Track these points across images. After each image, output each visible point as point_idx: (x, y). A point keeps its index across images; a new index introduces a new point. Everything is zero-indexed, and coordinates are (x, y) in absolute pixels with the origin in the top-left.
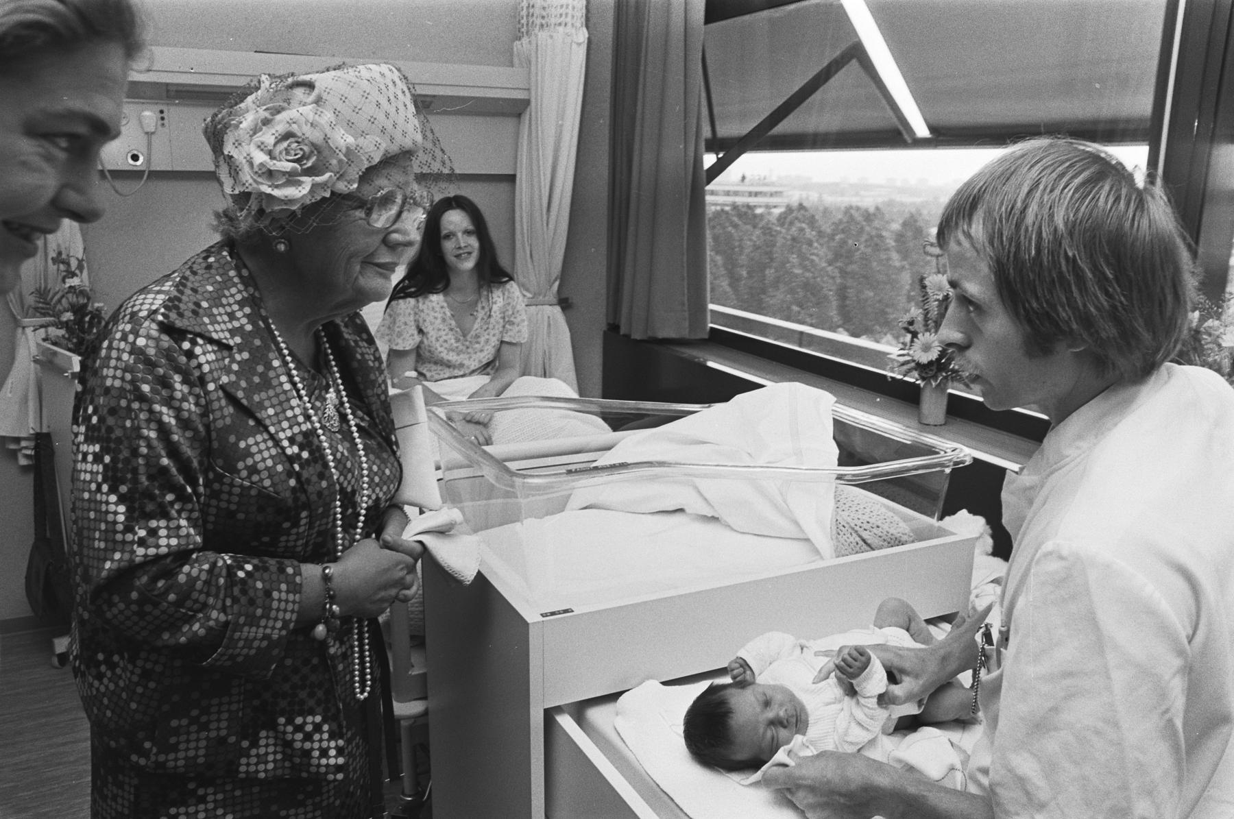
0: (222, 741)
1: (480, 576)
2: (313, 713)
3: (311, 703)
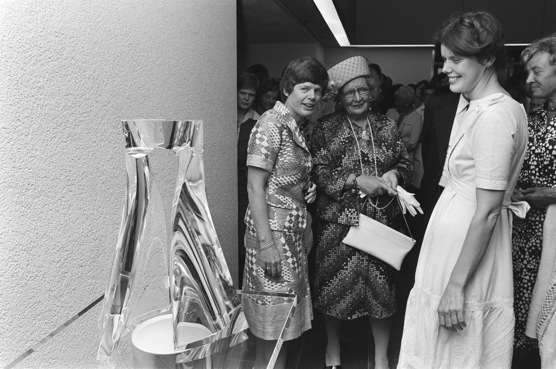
0: (335, 213)
1: (442, 189)
2: (353, 208)
3: (353, 206)
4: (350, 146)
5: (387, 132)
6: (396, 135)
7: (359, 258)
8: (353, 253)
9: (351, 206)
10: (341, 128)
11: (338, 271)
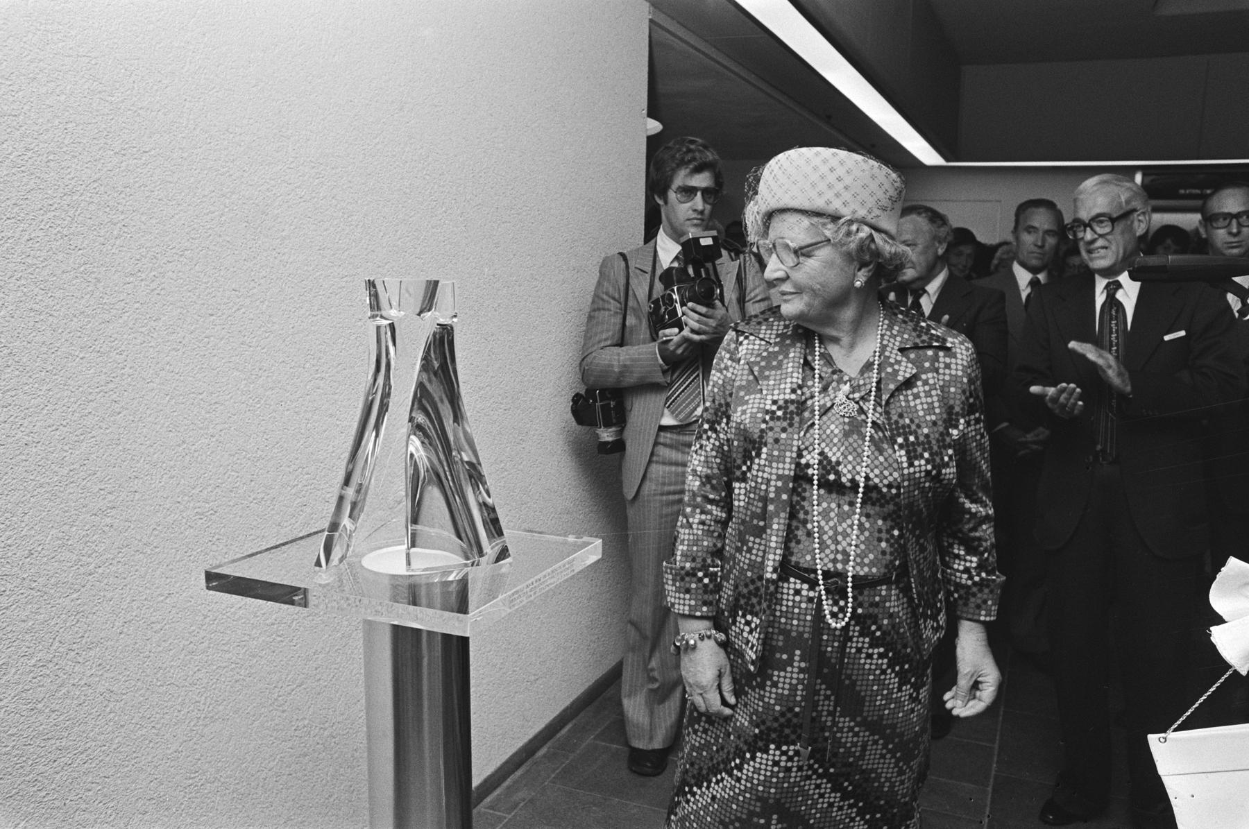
4: (784, 430)
5: (928, 394)
6: (952, 407)
7: (776, 763)
8: (760, 744)
9: (753, 606)
10: (779, 366)
11: (715, 771)
